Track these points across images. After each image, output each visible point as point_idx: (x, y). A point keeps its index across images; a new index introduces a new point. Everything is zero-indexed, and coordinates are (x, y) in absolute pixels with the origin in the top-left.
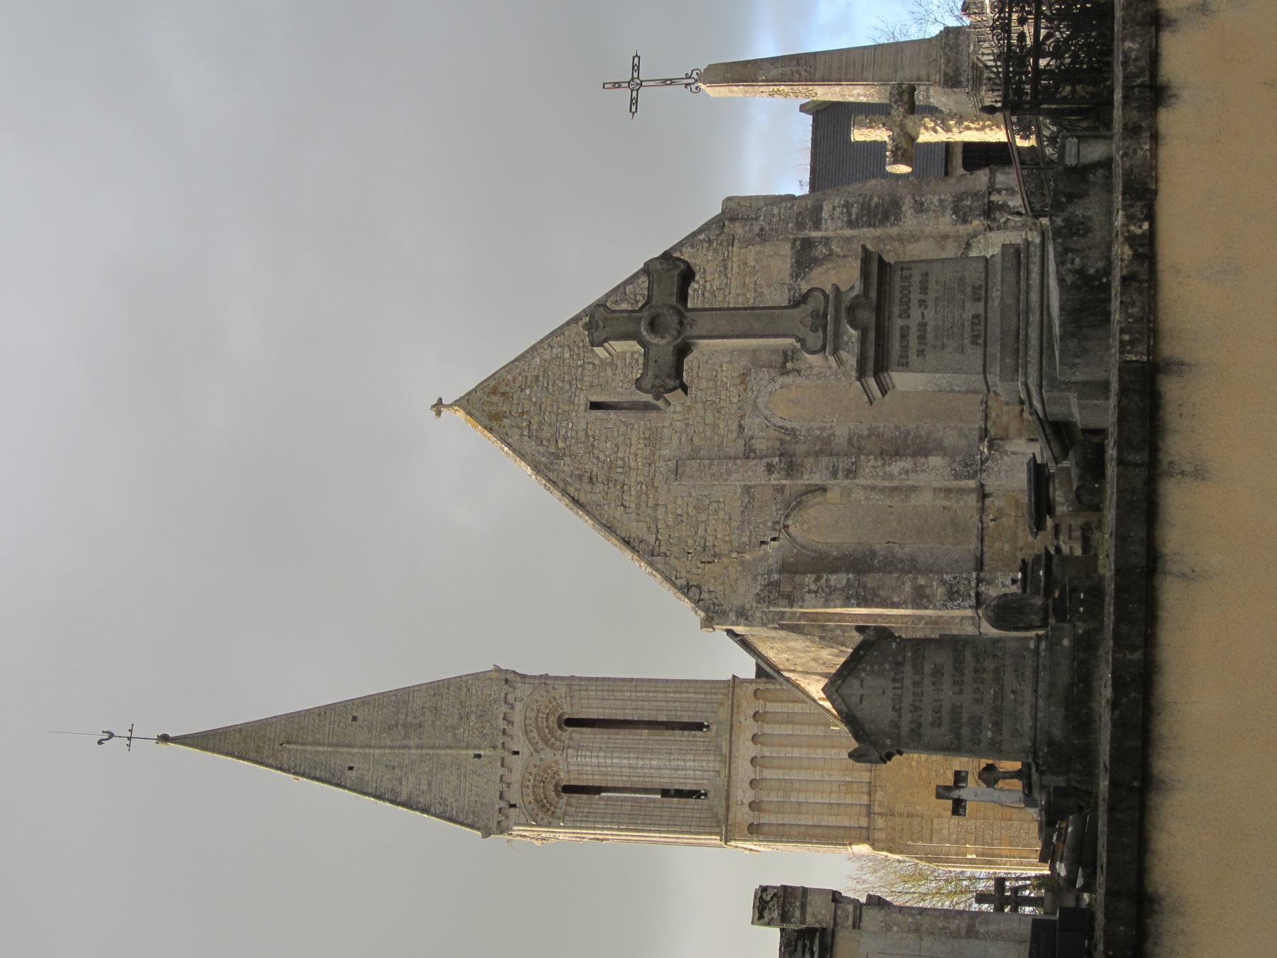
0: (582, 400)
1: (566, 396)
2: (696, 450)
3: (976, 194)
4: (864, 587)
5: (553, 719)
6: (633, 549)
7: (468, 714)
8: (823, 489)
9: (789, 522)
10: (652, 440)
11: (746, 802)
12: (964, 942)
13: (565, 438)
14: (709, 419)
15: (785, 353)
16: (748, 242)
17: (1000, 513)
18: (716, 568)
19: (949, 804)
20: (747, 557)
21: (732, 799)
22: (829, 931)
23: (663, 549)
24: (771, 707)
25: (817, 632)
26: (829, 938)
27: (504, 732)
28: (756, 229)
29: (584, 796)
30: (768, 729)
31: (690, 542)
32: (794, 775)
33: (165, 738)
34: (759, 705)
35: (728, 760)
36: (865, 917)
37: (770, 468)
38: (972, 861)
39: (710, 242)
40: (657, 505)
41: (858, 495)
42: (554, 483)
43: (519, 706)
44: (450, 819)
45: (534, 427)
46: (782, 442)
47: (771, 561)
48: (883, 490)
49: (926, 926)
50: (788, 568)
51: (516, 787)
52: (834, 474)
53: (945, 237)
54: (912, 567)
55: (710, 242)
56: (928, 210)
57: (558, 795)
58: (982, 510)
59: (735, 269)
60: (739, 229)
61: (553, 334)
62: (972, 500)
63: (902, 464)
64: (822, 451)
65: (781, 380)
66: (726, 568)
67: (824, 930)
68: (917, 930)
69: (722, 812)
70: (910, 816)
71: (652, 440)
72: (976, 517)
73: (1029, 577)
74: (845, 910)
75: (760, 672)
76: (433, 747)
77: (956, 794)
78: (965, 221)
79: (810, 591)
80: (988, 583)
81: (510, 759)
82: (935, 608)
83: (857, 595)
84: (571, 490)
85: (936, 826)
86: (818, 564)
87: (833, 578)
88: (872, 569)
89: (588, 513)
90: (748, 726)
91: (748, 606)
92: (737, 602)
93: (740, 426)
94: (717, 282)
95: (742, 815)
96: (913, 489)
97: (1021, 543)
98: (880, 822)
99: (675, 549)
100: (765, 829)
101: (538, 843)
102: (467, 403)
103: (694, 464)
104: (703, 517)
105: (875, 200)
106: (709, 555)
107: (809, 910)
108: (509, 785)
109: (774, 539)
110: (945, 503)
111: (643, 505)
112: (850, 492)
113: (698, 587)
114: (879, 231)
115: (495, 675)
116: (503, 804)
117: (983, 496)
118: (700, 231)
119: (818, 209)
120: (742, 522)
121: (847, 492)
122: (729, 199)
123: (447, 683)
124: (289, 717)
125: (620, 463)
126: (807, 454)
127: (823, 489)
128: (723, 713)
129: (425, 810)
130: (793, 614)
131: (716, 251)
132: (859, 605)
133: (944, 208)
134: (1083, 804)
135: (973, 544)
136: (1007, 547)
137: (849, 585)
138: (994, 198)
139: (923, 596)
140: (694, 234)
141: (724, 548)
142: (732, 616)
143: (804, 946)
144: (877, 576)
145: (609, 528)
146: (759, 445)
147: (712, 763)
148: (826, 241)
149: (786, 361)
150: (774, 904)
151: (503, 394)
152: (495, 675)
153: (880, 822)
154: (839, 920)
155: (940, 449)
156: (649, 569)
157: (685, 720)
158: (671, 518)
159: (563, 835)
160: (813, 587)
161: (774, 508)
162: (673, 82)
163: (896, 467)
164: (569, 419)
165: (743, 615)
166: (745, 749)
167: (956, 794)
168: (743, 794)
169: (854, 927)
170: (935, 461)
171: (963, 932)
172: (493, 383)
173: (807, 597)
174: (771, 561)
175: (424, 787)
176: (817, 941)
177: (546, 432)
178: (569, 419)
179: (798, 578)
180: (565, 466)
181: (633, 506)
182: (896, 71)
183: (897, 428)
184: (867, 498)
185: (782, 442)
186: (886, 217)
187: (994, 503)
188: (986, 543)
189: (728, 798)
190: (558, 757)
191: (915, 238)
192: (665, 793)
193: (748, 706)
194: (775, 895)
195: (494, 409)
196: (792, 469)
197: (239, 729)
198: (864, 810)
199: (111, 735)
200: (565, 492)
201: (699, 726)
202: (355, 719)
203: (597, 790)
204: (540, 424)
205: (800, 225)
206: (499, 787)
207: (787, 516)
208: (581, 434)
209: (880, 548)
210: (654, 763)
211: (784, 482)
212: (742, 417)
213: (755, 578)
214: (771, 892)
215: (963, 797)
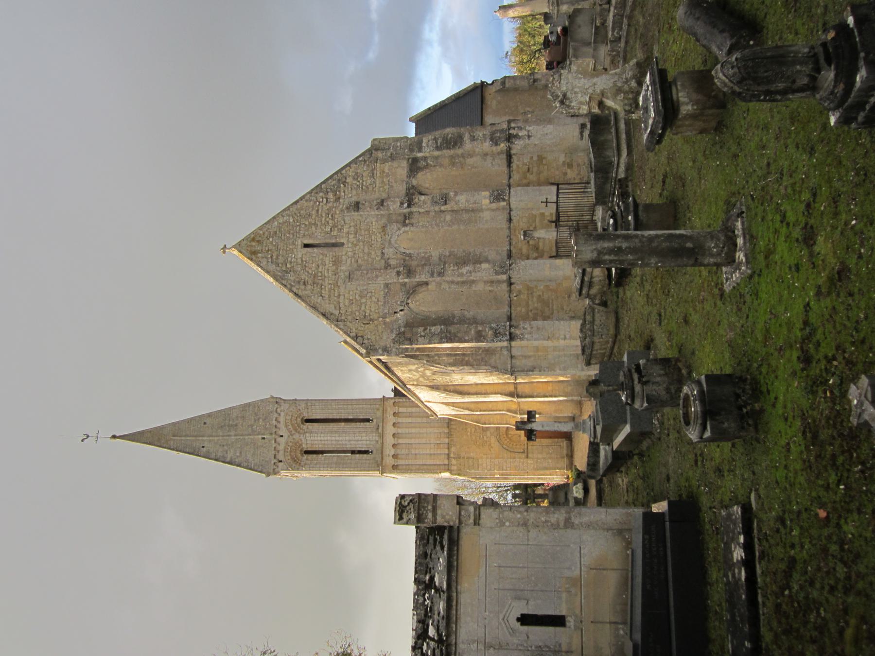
0: (299, 242)
1: (291, 241)
2: (360, 266)
3: (502, 130)
4: (450, 333)
5: (299, 420)
6: (327, 318)
7: (259, 419)
8: (427, 284)
9: (409, 301)
10: (337, 262)
11: (391, 455)
12: (562, 532)
13: (291, 262)
14: (366, 250)
15: (405, 216)
16: (384, 161)
17: (520, 292)
18: (371, 326)
20: (388, 320)
21: (384, 453)
22: (456, 527)
23: (343, 318)
24: (401, 410)
25: (426, 358)
26: (456, 534)
27: (276, 426)
28: (389, 154)
29: (315, 456)
30: (400, 420)
32: (412, 441)
33: (114, 437)
34: (396, 409)
35: (382, 436)
36: (483, 516)
37: (398, 273)
38: (497, 478)
39: (365, 161)
41: (445, 286)
42: (285, 286)
43: (282, 414)
44: (251, 469)
45: (274, 257)
46: (404, 260)
47: (400, 322)
48: (458, 283)
49: (531, 521)
50: (408, 325)
51: (281, 453)
52: (432, 275)
53: (486, 155)
54: (475, 321)
55: (365, 161)
56: (477, 139)
57: (302, 455)
58: (510, 291)
59: (378, 175)
60: (380, 154)
61: (284, 210)
62: (504, 286)
63: (467, 268)
64: (425, 265)
65: (403, 229)
66: (376, 326)
67: (451, 527)
68: (525, 524)
69: (379, 460)
70: (468, 458)
71: (337, 262)
72: (507, 295)
73: (620, 222)
74: (467, 510)
75: (396, 392)
76: (242, 435)
77: (529, 426)
78: (497, 144)
79: (421, 336)
81: (279, 439)
82: (487, 342)
83: (446, 337)
84: (294, 289)
85: (480, 462)
86: (425, 322)
87: (433, 328)
88: (453, 323)
89: (303, 300)
90: (391, 419)
92: (382, 344)
93: (383, 253)
94: (369, 181)
95: (389, 461)
96: (473, 282)
97: (531, 308)
98: (454, 462)
99: (349, 318)
100: (400, 467)
101: (295, 479)
102: (238, 246)
103: (359, 273)
104: (364, 300)
105: (450, 136)
106: (367, 320)
107: (439, 512)
108: (278, 451)
110: (490, 288)
111: (332, 296)
112: (441, 284)
113: (362, 337)
114: (452, 152)
115: (271, 400)
116: (275, 461)
117: (511, 284)
118: (360, 156)
119: (420, 143)
120: (385, 302)
121: (439, 284)
122: (374, 140)
123: (249, 405)
124: (174, 424)
126: (418, 266)
127: (427, 284)
128: (379, 414)
129: (239, 465)
130: (413, 349)
131: (368, 165)
132: (447, 342)
134: (739, 391)
135: (506, 309)
136: (523, 310)
137: (441, 332)
138: (512, 131)
139: (481, 336)
140: (357, 158)
141: (375, 316)
142: (380, 351)
143: (435, 540)
144: (456, 326)
145: (314, 308)
146: (393, 262)
147: (374, 437)
148: (425, 158)
149: (406, 219)
150: (409, 507)
151: (258, 241)
152: (271, 400)
153: (454, 462)
154: (463, 519)
155: (487, 261)
156: (336, 329)
157: (361, 417)
158: (347, 302)
159: (305, 474)
160: (423, 334)
163: (464, 270)
164: (293, 253)
165: (386, 351)
166: (390, 430)
168: (389, 451)
169: (475, 524)
170: (485, 266)
171: (562, 524)
172: (252, 236)
173: (420, 339)
174: (400, 322)
175: (238, 454)
176: (446, 537)
177: (281, 260)
178: (293, 253)
179: (414, 330)
180: (291, 277)
184: (450, 288)
185: (404, 260)
186: (455, 144)
187: (516, 287)
188: (513, 308)
189: (382, 453)
190: (302, 437)
191: (471, 156)
192: (353, 452)
193: (390, 411)
194: (411, 501)
195: (253, 249)
196: (410, 273)
197: (150, 431)
198: (446, 456)
199: (88, 436)
200: (291, 290)
201: (368, 420)
202: (205, 423)
203: (322, 452)
204: (278, 256)
205: (411, 150)
206: (273, 452)
207: (408, 298)
208: (299, 261)
209: (457, 313)
210: (347, 438)
211: (406, 280)
212: (383, 248)
213: (392, 331)
214: (408, 499)
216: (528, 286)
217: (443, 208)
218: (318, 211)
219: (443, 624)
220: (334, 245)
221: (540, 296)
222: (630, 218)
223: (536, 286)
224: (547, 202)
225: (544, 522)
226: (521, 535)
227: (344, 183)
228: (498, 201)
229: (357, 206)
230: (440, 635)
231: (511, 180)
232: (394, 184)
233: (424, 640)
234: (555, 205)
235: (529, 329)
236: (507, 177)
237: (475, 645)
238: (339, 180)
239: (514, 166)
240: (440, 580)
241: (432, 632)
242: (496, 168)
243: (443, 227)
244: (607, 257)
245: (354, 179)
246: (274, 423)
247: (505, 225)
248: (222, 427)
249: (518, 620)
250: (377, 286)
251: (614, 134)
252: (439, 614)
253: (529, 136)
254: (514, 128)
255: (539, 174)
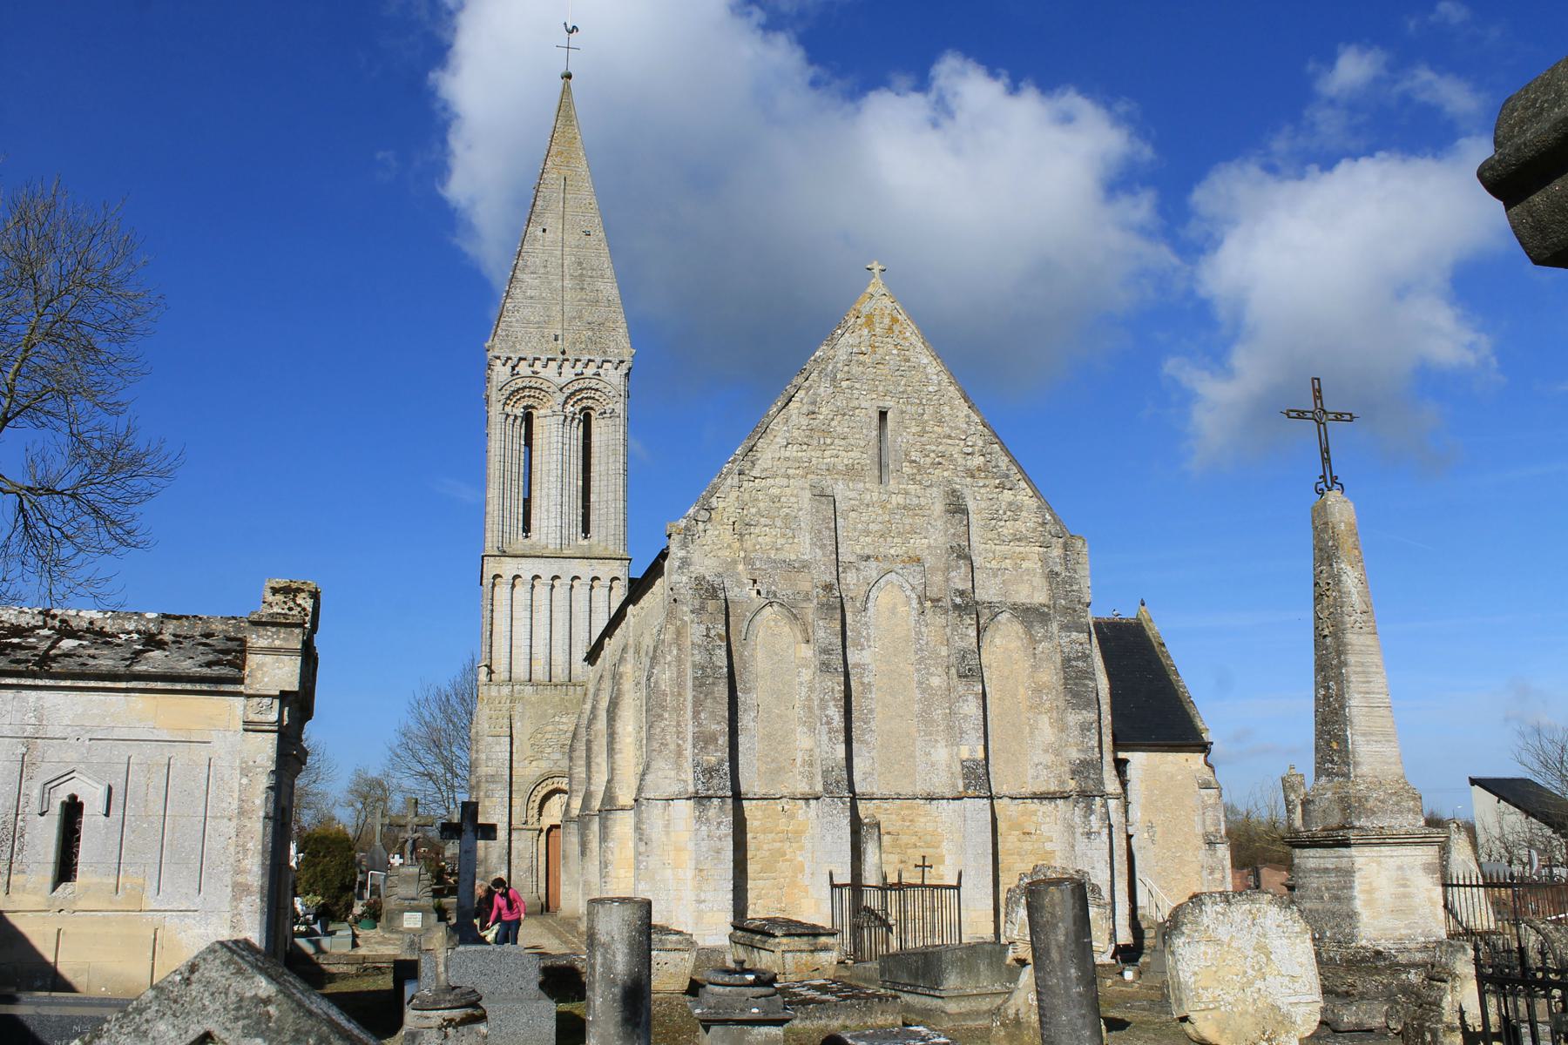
0: (888, 403)
3: (1101, 782)
5: (590, 403)
9: (776, 607)
10: (852, 472)
12: (228, 879)
16: (1044, 560)
17: (792, 817)
18: (728, 536)
19: (456, 818)
20: (741, 567)
23: (745, 484)
28: (1057, 569)
31: (753, 510)
37: (828, 588)
40: (789, 477)
45: (861, 357)
56: (1084, 736)
59: (1018, 549)
67: (241, 681)
68: (242, 812)
71: (852, 472)
72: (785, 792)
77: (467, 827)
79: (708, 629)
80: (721, 808)
82: (695, 755)
91: (692, 568)
92: (696, 557)
94: (1005, 531)
99: (746, 496)
104: (779, 523)
105: (1091, 684)
107: (269, 659)
109: (759, 592)
110: (799, 762)
125: (829, 441)
131: (1035, 530)
133: (1085, 751)
137: (715, 668)
141: (748, 544)
151: (890, 329)
157: (592, 517)
160: (713, 633)
161: (789, 592)
162: (1326, 460)
167: (467, 827)
171: (240, 879)
177: (856, 370)
178: (870, 391)
181: (788, 454)
182: (1364, 735)
183: (871, 711)
195: (877, 319)
201: (586, 529)
208: (856, 403)
213: (719, 575)
215: (464, 837)
216: (803, 832)
217: (953, 671)
218: (949, 437)
219: (71, 664)
220: (881, 466)
221: (784, 854)
222: (755, 1010)
223: (802, 848)
224: (924, 866)
225: (243, 846)
226: (224, 805)
227: (1001, 486)
228: (965, 776)
229: (957, 508)
230: (55, 659)
231: (1006, 800)
232: (998, 580)
233: (58, 631)
234: (919, 882)
235: (718, 833)
236: (1014, 793)
237: (33, 721)
238: (1007, 476)
239: (1034, 805)
240: (156, 660)
241: (68, 644)
242: (1031, 772)
243: (918, 670)
244: (599, 959)
245: (1010, 504)
246: (585, 358)
247: (920, 789)
248: (580, 264)
249: (73, 798)
250: (804, 547)
251: (991, 989)
252: (94, 657)
253: (1089, 834)
254: (1105, 805)
255: (1019, 854)
